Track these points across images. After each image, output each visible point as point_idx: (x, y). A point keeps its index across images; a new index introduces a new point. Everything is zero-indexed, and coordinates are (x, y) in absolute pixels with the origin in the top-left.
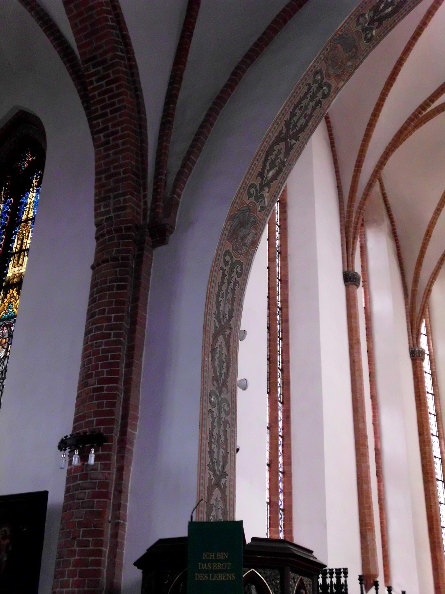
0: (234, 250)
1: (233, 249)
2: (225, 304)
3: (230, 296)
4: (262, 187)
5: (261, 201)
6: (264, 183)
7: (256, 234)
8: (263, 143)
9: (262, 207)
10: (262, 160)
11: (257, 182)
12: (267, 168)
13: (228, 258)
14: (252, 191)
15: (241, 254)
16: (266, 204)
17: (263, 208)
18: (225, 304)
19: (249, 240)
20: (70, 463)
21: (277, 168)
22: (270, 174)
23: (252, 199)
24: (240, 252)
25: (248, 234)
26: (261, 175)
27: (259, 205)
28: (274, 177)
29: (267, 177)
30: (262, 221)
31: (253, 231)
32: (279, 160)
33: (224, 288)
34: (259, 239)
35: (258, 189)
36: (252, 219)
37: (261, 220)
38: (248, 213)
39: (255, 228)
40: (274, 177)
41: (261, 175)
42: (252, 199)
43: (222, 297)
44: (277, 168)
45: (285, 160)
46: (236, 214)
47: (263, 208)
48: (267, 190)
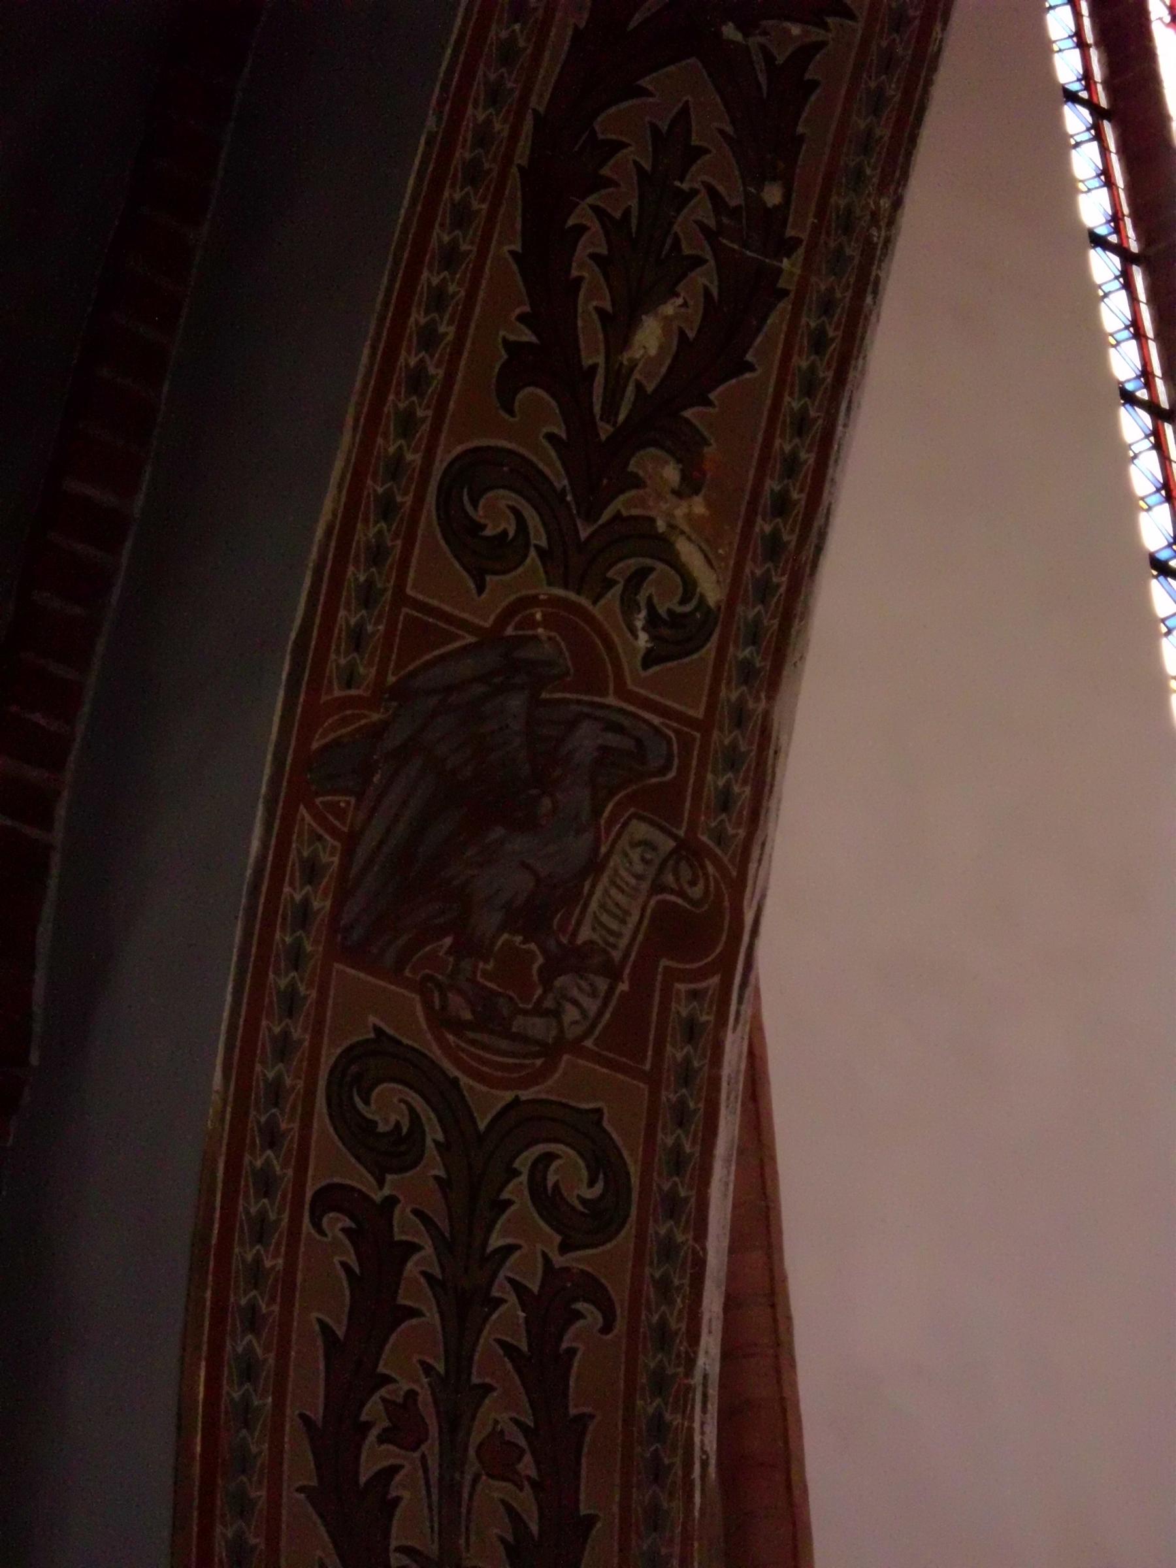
0: (458, 1026)
1: (441, 1021)
2: (450, 1491)
3: (502, 1413)
4: (600, 465)
5: (638, 578)
6: (605, 430)
7: (689, 852)
8: (458, 113)
9: (676, 620)
10: (506, 246)
11: (535, 427)
12: (594, 299)
13: (389, 1105)
14: (497, 511)
15: (552, 1051)
16: (712, 590)
17: (678, 634)
18: (450, 1491)
19: (614, 909)
20: (1129, 381)
21: (704, 278)
22: (649, 338)
23: (529, 577)
24: (538, 1027)
25: (595, 866)
26: (547, 362)
27: (629, 605)
28: (711, 355)
29: (618, 378)
30: (722, 737)
31: (641, 830)
32: (701, 211)
33: (408, 1363)
34: (739, 885)
35: (562, 482)
36: (586, 741)
37: (705, 726)
38: (516, 703)
39: (662, 805)
40: (711, 355)
41: (547, 362)
42: (529, 577)
43: (404, 1427)
44: (704, 278)
45: (773, 195)
46: (377, 732)
47: (678, 634)
48: (671, 473)
